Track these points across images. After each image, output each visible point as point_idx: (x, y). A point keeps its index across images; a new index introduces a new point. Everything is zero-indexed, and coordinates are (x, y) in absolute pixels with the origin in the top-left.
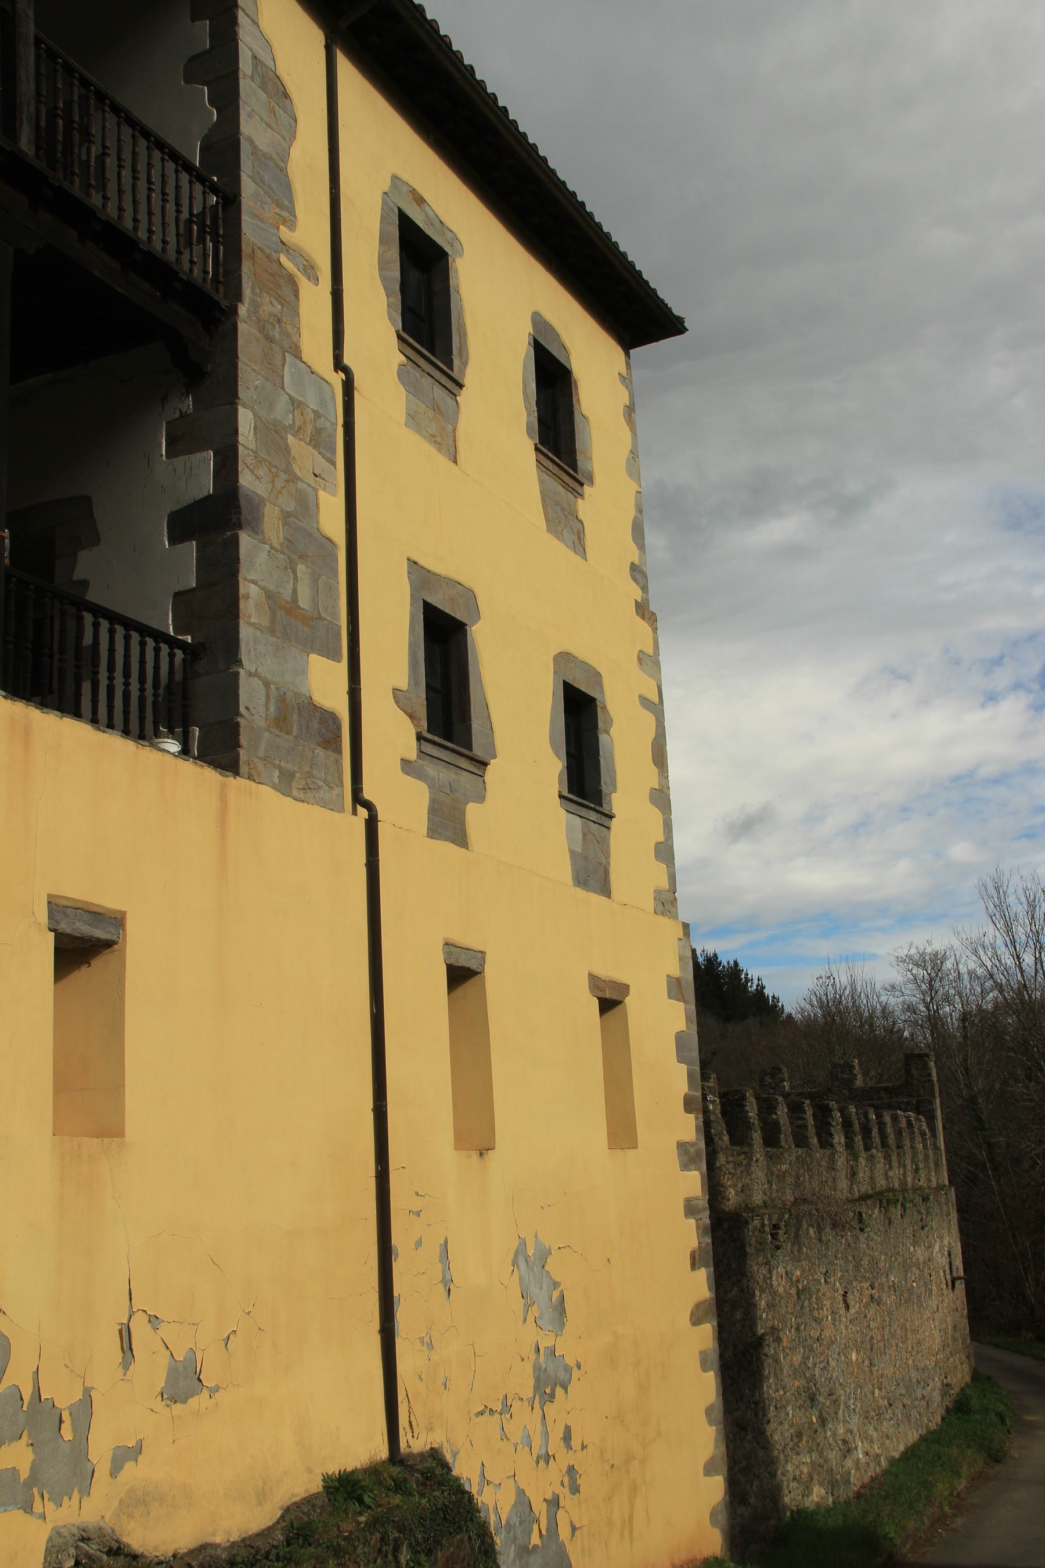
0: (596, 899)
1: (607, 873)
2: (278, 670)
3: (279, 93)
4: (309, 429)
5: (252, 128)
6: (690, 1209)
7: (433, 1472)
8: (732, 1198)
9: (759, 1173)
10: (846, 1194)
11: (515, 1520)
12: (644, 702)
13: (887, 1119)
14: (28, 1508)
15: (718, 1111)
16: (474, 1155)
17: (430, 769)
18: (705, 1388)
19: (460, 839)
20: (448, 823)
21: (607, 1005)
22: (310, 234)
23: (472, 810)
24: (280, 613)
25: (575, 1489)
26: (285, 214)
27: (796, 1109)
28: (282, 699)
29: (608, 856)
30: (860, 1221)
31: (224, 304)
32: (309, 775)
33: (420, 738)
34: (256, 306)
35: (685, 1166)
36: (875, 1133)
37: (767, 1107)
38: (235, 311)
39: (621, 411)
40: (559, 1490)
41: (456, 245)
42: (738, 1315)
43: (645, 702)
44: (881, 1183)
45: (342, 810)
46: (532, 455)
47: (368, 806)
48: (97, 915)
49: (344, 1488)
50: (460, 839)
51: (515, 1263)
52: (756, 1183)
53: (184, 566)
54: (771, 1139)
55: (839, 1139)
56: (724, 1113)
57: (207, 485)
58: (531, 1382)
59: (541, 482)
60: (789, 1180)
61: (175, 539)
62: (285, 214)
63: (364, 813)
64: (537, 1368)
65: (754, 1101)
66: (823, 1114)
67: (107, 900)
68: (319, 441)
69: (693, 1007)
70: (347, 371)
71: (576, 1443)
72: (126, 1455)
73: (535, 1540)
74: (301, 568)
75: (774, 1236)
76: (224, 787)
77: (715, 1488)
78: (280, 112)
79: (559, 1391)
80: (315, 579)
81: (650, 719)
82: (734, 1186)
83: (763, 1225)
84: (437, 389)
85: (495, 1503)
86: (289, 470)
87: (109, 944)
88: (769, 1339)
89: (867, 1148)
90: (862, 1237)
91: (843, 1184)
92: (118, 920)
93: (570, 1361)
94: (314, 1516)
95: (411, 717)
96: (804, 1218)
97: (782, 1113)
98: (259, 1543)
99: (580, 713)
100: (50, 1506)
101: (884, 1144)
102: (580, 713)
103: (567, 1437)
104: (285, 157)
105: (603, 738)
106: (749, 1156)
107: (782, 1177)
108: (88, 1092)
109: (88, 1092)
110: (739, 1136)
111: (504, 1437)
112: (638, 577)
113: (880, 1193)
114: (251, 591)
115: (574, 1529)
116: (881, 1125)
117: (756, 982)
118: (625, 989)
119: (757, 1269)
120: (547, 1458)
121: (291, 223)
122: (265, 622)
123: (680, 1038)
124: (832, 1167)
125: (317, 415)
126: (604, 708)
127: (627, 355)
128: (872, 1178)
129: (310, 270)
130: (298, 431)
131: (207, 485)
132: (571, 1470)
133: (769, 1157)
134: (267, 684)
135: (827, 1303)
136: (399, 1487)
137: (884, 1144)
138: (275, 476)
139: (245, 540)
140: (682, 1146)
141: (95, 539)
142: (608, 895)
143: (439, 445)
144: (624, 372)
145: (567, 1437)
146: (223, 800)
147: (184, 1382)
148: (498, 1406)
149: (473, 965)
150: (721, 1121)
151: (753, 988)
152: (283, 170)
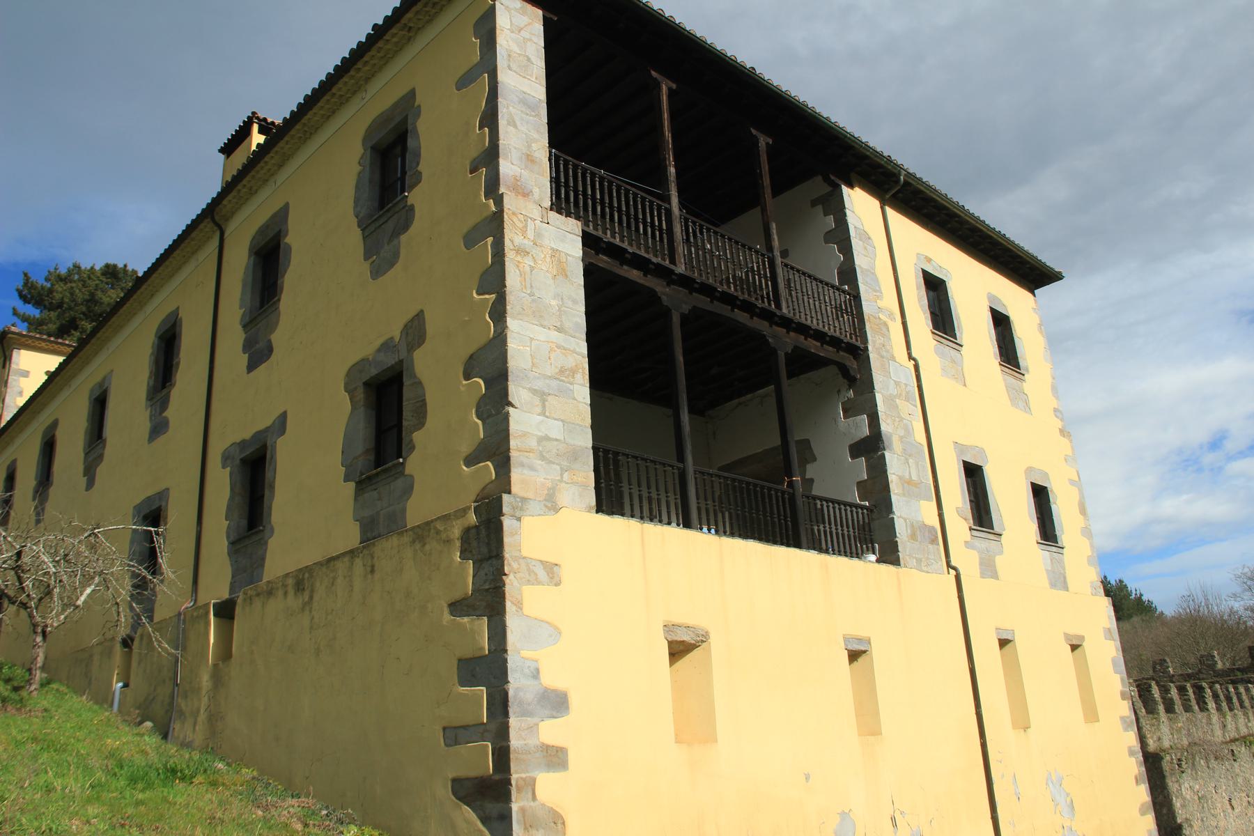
2: (910, 511)
3: (866, 238)
5: (860, 261)
8: (1152, 745)
10: (1221, 739)
13: (1242, 690)
17: (977, 543)
19: (995, 575)
21: (1074, 648)
23: (998, 559)
27: (1182, 690)
28: (912, 525)
30: (1233, 755)
33: (971, 529)
34: (874, 342)
35: (1126, 730)
36: (1235, 700)
37: (1165, 690)
44: (1244, 731)
46: (999, 368)
47: (955, 568)
48: (860, 640)
50: (995, 575)
52: (1165, 734)
53: (861, 468)
54: (1170, 709)
55: (1211, 705)
56: (1140, 696)
60: (1184, 732)
61: (853, 457)
66: (1199, 690)
67: (863, 633)
70: (914, 359)
74: (911, 461)
75: (1180, 765)
87: (865, 652)
88: (1185, 826)
89: (1231, 709)
90: (1236, 765)
91: (1218, 732)
96: (1194, 752)
97: (1174, 693)
101: (1242, 706)
104: (873, 267)
106: (1158, 719)
107: (1179, 730)
108: (868, 718)
109: (868, 718)
113: (1244, 737)
116: (1238, 694)
119: (1172, 785)
124: (1209, 723)
128: (1237, 728)
129: (891, 316)
130: (899, 396)
135: (1219, 805)
137: (1242, 706)
139: (887, 454)
140: (1122, 718)
142: (1066, 588)
152: (874, 274)
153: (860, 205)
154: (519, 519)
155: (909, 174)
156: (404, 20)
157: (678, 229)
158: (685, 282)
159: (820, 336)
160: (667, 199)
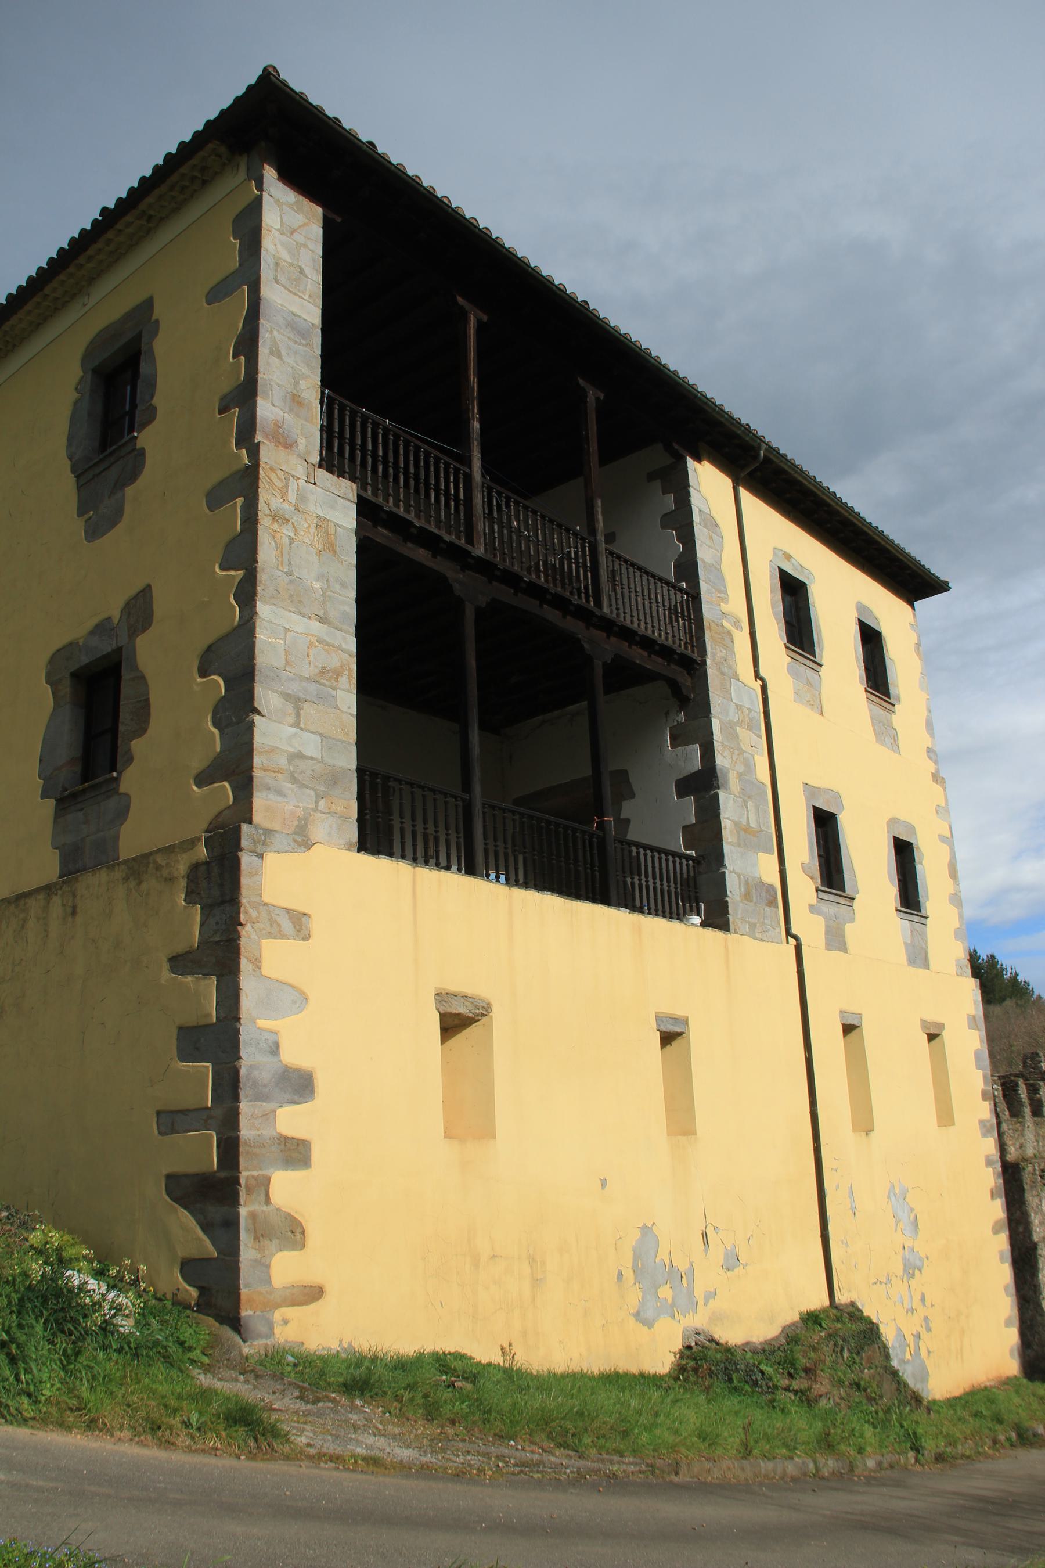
0: (922, 972)
1: (926, 953)
3: (713, 525)
4: (747, 720)
5: (703, 553)
6: (989, 1163)
7: (854, 1313)
9: (1030, 1135)
11: (897, 1345)
12: (942, 839)
14: (673, 1317)
15: (1001, 1096)
16: (863, 1134)
17: (825, 907)
18: (1005, 1273)
19: (843, 947)
20: (836, 940)
21: (931, 1037)
22: (736, 604)
23: (848, 928)
24: (742, 833)
25: (929, 1330)
26: (722, 595)
28: (747, 883)
29: (926, 943)
31: (698, 659)
32: (763, 923)
33: (817, 890)
34: (714, 655)
35: (984, 1135)
38: (704, 663)
39: (913, 648)
40: (920, 1329)
41: (811, 577)
42: (1021, 1229)
43: (942, 839)
45: (779, 942)
47: (795, 937)
48: (675, 1020)
49: (812, 1319)
50: (843, 947)
51: (889, 1197)
53: (688, 810)
56: (1004, 1096)
57: (698, 765)
58: (901, 1267)
59: (870, 710)
61: (680, 795)
62: (722, 595)
63: (793, 941)
64: (904, 1259)
65: (1024, 1086)
67: (680, 1012)
68: (751, 726)
69: (984, 1033)
70: (762, 679)
71: (928, 1303)
72: (710, 1295)
73: (908, 1356)
74: (750, 803)
76: (726, 940)
77: (1012, 1336)
78: (715, 536)
79: (917, 1271)
80: (757, 808)
81: (945, 848)
82: (1014, 1145)
83: (1034, 1170)
84: (809, 671)
85: (888, 1334)
86: (739, 749)
87: (680, 1034)
92: (685, 1022)
93: (922, 1255)
94: (798, 1332)
95: (812, 878)
98: (773, 1343)
99: (904, 852)
100: (681, 1317)
102: (904, 852)
103: (923, 1299)
104: (719, 562)
105: (918, 867)
106: (1023, 1124)
110: (1015, 1112)
111: (888, 1297)
112: (932, 755)
114: (727, 824)
115: (929, 1352)
117: (1009, 970)
118: (942, 1026)
120: (912, 1310)
121: (725, 600)
122: (735, 841)
123: (977, 1055)
125: (750, 710)
126: (918, 848)
127: (913, 608)
131: (698, 765)
132: (926, 1318)
133: (1036, 1124)
134: (739, 876)
136: (838, 1320)
138: (733, 753)
139: (722, 794)
140: (982, 1122)
141: (632, 795)
142: (927, 966)
143: (810, 704)
144: (912, 621)
145: (923, 1299)
146: (726, 947)
147: (732, 1261)
148: (884, 1280)
149: (856, 1023)
150: (1003, 1102)
151: (1007, 976)
152: (719, 570)
153: (709, 484)
154: (261, 856)
155: (771, 449)
156: (143, 206)
157: (478, 500)
158: (484, 567)
159: (647, 644)
160: (467, 462)
